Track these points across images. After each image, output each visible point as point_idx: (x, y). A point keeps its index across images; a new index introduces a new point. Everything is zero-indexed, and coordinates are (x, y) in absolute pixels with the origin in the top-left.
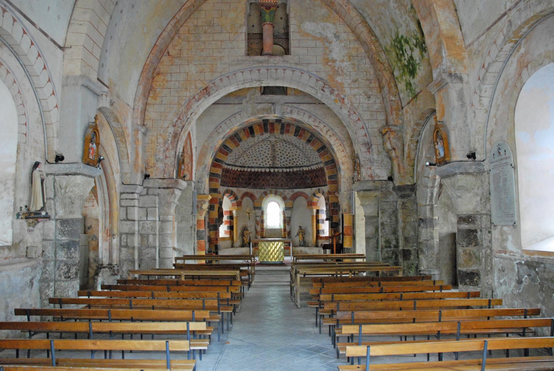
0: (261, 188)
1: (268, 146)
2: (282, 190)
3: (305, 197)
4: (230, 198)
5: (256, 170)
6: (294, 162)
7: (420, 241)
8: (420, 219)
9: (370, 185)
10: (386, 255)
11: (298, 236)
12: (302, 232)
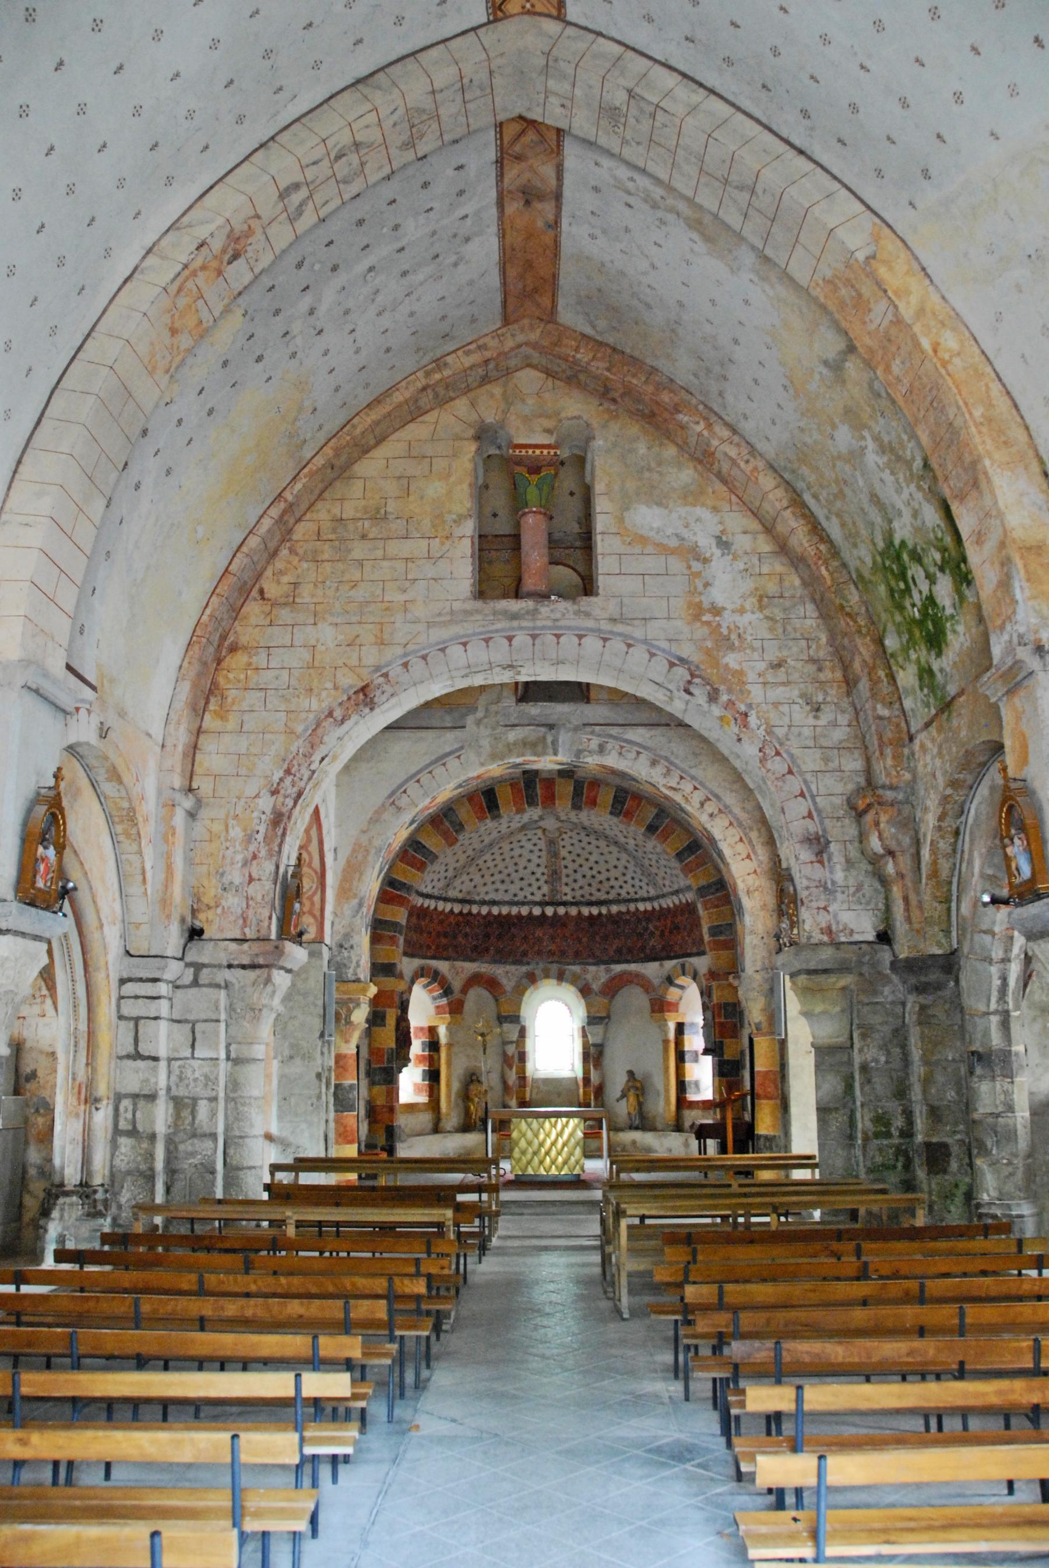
0: (514, 963)
4: (431, 991)
5: (505, 910)
7: (976, 1116)
8: (973, 1053)
9: (827, 955)
10: (879, 1159)
12: (637, 1089)
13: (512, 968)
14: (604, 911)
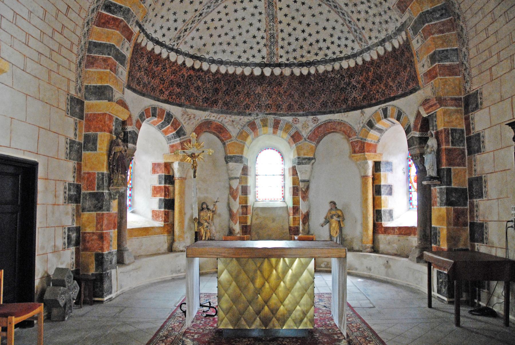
0: (239, 114)
2: (290, 119)
3: (345, 132)
4: (165, 132)
5: (231, 70)
6: (320, 49)
11: (327, 225)
12: (339, 216)
13: (237, 118)
14: (313, 71)
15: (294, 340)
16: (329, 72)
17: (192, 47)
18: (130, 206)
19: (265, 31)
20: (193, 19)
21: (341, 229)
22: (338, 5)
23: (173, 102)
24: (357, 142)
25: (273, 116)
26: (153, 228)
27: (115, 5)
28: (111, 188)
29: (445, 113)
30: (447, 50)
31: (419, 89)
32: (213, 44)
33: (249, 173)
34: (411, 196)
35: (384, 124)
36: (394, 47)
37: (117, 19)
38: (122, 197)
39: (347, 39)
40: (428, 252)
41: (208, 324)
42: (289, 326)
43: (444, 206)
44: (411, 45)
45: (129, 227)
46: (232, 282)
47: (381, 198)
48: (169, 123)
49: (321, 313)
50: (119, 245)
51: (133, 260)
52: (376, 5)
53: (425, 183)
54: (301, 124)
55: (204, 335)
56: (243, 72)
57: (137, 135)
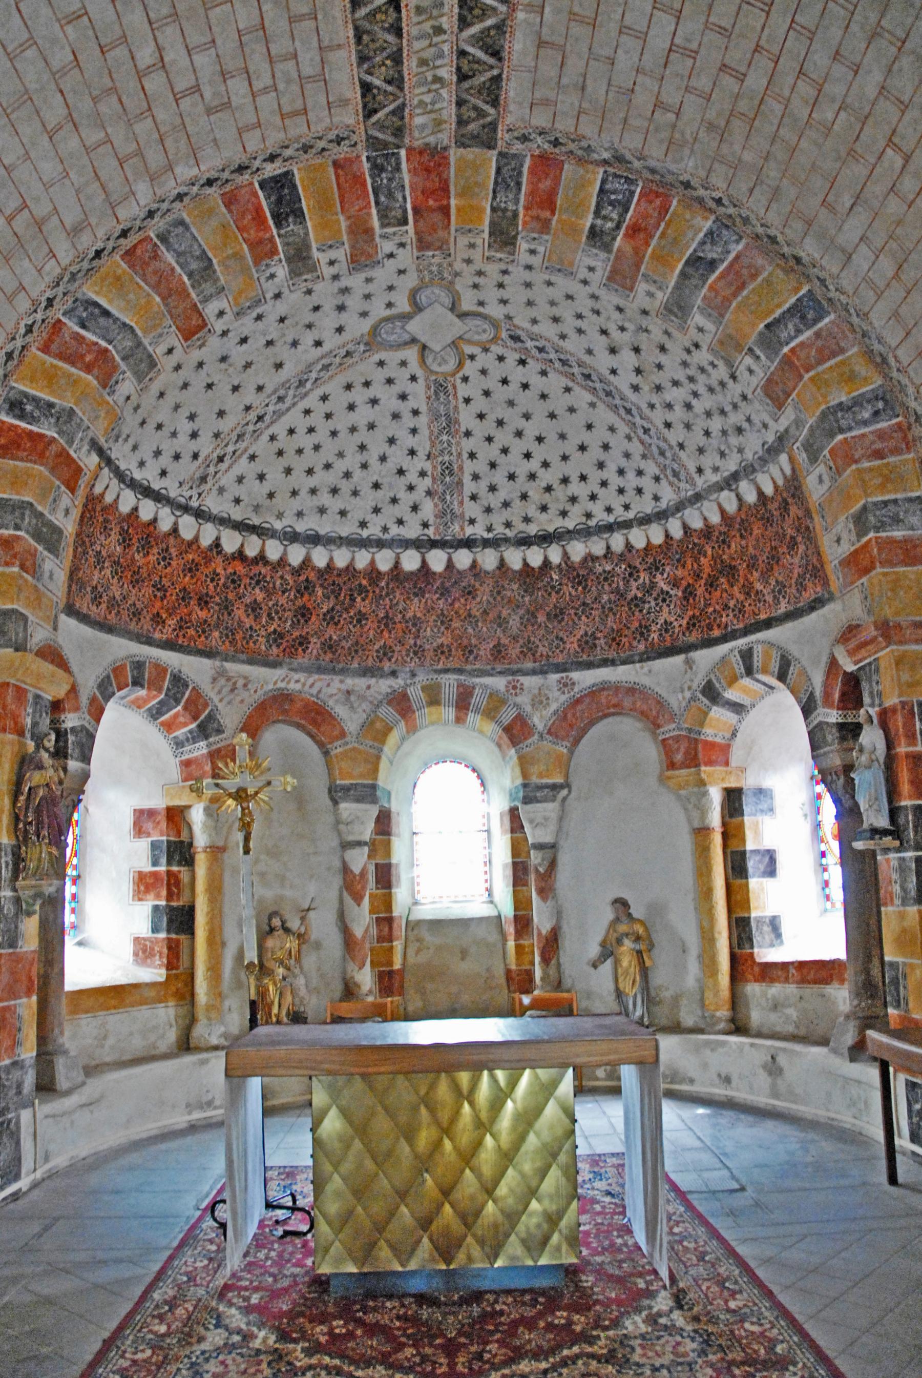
0: (366, 672)
1: (410, 388)
2: (499, 683)
4: (168, 727)
6: (573, 500)
11: (609, 964)
12: (638, 938)
13: (359, 683)
15: (527, 1297)
16: (597, 558)
17: (237, 501)
18: (73, 927)
19: (429, 457)
20: (238, 429)
21: (644, 971)
22: (614, 391)
23: (188, 645)
24: (677, 739)
25: (456, 677)
26: (136, 986)
27: (35, 400)
28: (20, 883)
29: (899, 661)
30: (895, 501)
31: (831, 598)
32: (294, 493)
33: (394, 830)
34: (826, 876)
35: (745, 690)
36: (760, 493)
37: (42, 436)
38: (55, 903)
39: (640, 473)
40: (880, 1031)
41: (288, 1261)
42: (513, 1258)
43: (913, 905)
44: (804, 487)
45: (68, 987)
46: (352, 1138)
47: (747, 885)
48: (178, 702)
49: (599, 1213)
50: (42, 1040)
51: (81, 1078)
52: (711, 390)
53: (859, 845)
54: (530, 696)
55: (276, 1294)
56: (373, 562)
57: (92, 737)
